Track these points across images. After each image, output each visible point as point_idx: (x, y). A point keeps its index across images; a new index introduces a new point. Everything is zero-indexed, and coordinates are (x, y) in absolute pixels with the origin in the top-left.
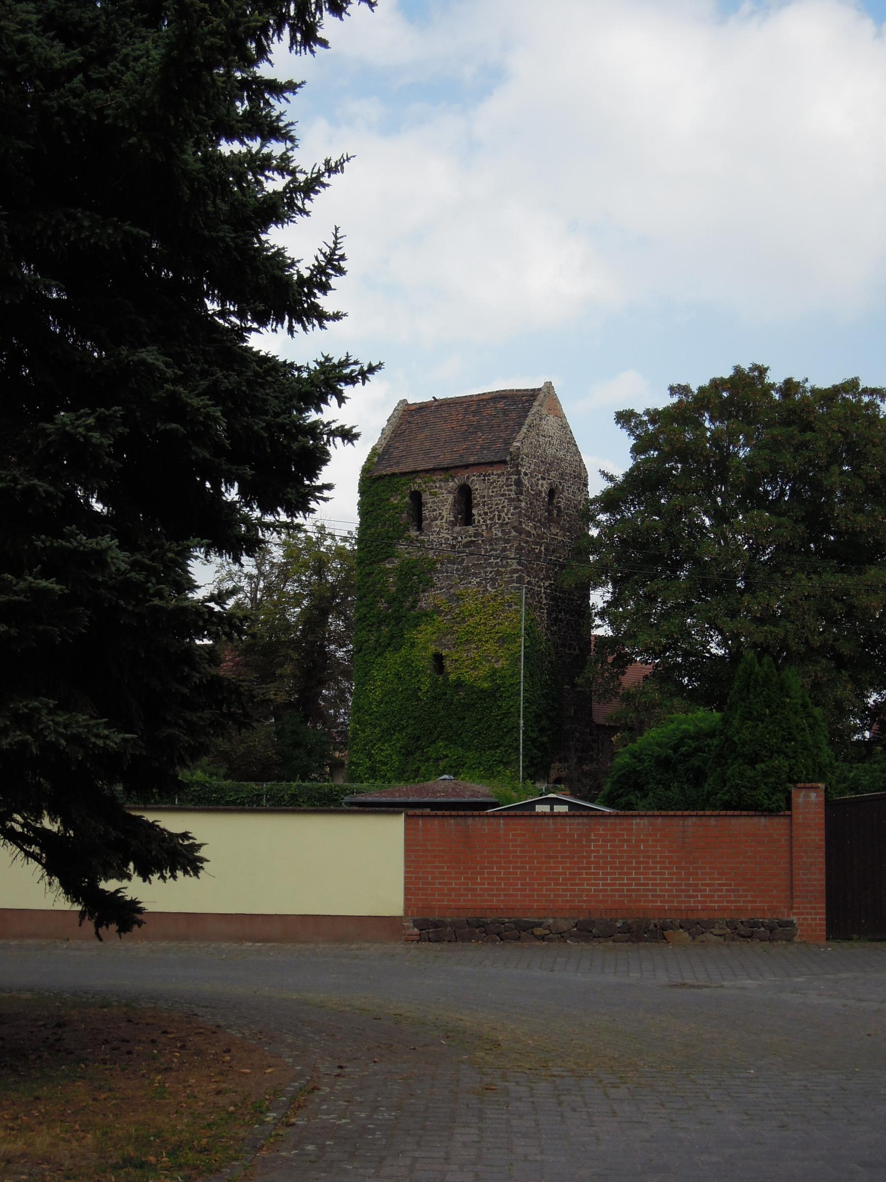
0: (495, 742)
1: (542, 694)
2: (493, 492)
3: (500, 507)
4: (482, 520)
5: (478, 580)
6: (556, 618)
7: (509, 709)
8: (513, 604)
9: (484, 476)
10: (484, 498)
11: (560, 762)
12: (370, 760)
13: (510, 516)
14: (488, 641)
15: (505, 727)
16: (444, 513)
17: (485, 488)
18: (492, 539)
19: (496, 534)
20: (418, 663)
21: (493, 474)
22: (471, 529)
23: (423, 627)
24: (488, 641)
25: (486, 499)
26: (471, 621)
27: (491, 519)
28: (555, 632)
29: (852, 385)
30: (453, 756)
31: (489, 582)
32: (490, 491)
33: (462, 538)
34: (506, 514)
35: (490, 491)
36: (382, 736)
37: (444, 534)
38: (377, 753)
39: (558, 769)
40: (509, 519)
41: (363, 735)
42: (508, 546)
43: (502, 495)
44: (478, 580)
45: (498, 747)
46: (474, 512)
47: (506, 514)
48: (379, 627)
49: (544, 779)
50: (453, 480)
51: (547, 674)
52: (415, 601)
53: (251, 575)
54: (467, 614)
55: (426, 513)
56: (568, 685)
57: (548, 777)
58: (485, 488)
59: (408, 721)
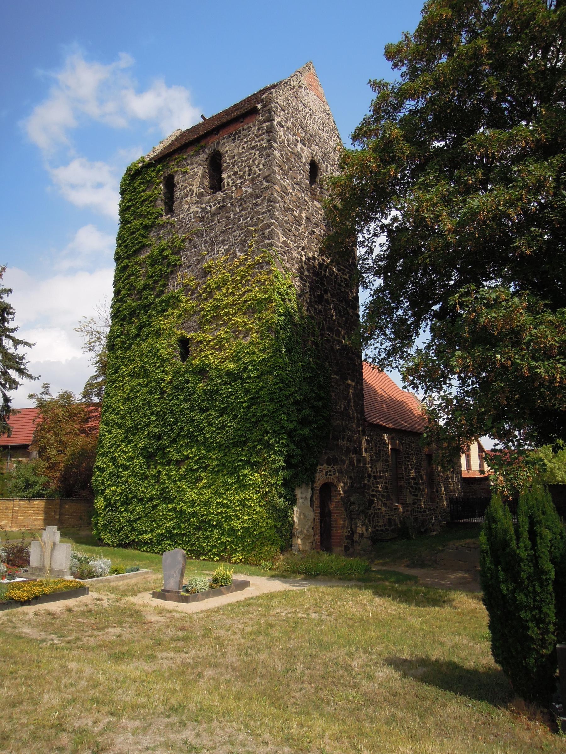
0: (240, 437)
1: (304, 378)
2: (243, 148)
3: (251, 161)
4: (231, 182)
5: (226, 247)
6: (321, 297)
7: (257, 392)
8: (264, 264)
9: (234, 135)
10: (234, 158)
11: (329, 464)
12: (114, 464)
13: (261, 167)
14: (236, 313)
15: (254, 416)
16: (195, 188)
17: (235, 147)
18: (241, 199)
19: (246, 191)
20: (162, 350)
21: (243, 129)
22: (220, 195)
23: (170, 311)
24: (236, 313)
25: (236, 158)
26: (218, 295)
27: (241, 177)
28: (320, 311)
29: (129, 170)
30: (195, 456)
31: (237, 247)
32: (240, 149)
33: (210, 206)
34: (257, 167)
35: (240, 149)
36: (126, 437)
37: (194, 208)
38: (119, 456)
39: (327, 473)
40: (260, 170)
41: (110, 436)
42: (259, 200)
43: (253, 148)
44: (226, 247)
45: (245, 443)
46: (224, 176)
47: (257, 167)
48: (130, 319)
49: (307, 485)
50: (204, 151)
51: (310, 356)
52: (164, 286)
53: (122, 223)
54: (214, 286)
55: (178, 194)
56: (337, 375)
57: (313, 482)
58: (235, 147)
59: (149, 418)
